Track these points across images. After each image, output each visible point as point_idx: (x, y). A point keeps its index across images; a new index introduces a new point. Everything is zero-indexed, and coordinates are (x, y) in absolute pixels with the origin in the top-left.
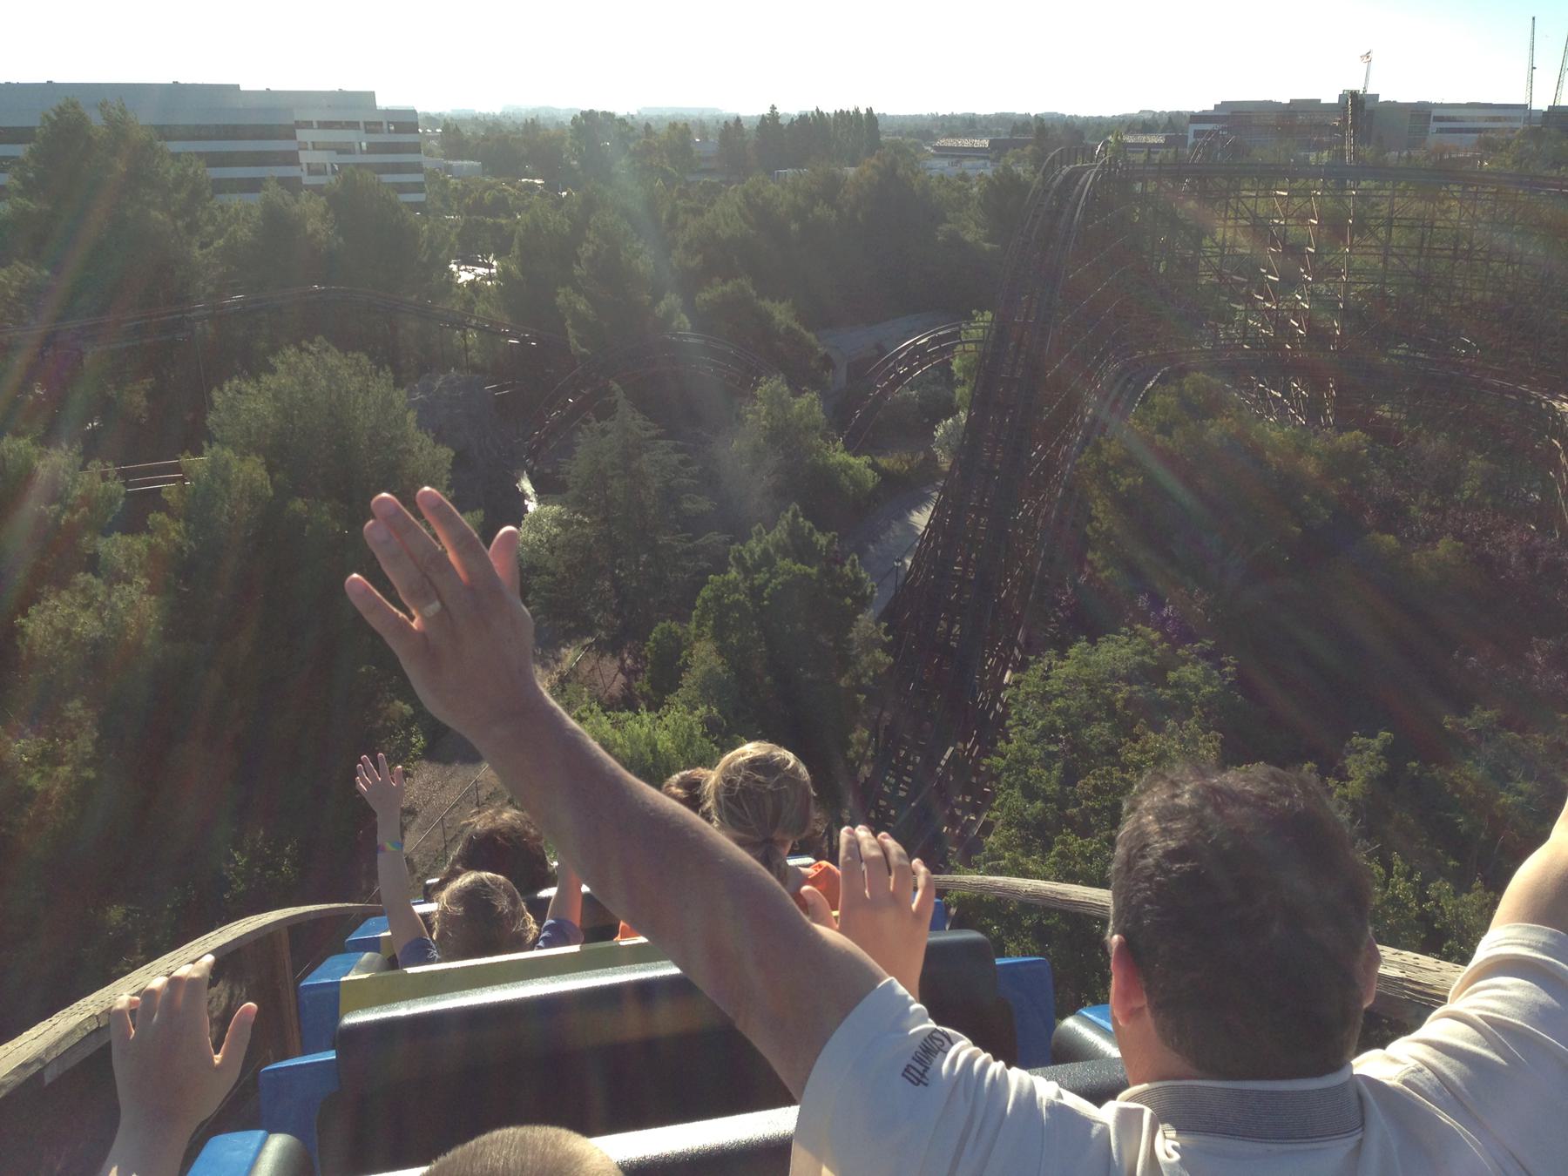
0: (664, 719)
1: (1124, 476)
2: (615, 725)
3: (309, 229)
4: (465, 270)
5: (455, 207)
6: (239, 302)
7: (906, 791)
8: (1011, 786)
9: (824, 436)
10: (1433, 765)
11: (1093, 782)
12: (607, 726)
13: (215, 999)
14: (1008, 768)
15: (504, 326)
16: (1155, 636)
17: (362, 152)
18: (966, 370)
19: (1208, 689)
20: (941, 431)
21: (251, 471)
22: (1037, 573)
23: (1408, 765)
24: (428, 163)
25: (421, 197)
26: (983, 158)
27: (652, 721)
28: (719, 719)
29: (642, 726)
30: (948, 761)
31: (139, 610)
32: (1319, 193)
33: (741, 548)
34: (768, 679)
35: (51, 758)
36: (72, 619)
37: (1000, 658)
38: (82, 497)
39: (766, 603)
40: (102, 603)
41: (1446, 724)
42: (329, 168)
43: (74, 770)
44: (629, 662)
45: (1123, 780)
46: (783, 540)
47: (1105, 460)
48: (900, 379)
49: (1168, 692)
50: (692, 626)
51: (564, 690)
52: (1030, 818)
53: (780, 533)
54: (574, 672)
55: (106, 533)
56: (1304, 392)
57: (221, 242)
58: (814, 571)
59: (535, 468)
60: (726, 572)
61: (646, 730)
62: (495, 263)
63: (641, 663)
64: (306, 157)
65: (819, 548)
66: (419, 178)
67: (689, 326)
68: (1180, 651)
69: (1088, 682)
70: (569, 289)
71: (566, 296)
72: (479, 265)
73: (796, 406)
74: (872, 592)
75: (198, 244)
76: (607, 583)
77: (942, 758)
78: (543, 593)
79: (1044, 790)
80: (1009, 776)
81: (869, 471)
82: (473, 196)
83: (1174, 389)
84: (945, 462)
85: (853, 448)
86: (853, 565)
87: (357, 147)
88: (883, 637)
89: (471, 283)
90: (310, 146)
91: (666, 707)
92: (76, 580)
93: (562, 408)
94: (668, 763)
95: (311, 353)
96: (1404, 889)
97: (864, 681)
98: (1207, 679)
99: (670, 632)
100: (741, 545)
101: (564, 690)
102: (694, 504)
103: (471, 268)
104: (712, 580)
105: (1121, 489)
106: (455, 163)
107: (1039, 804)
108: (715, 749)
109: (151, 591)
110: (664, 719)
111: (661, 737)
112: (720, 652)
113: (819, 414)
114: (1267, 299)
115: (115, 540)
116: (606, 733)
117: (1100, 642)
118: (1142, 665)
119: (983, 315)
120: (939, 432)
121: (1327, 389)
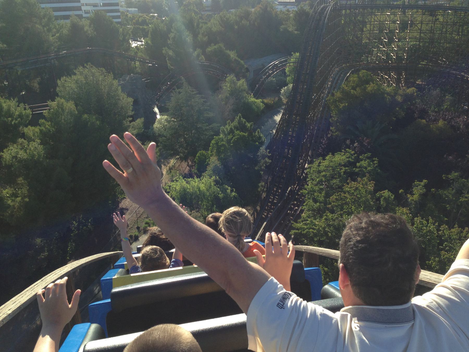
0: (202, 180)
1: (342, 103)
3: (85, 29)
4: (134, 43)
5: (130, 23)
6: (65, 53)
8: (309, 199)
9: (247, 93)
10: (439, 190)
11: (335, 197)
12: (185, 183)
14: (308, 193)
15: (147, 60)
16: (353, 152)
17: (101, 6)
20: (283, 91)
24: (121, 9)
25: (119, 20)
26: (293, 5)
27: (198, 181)
29: (195, 183)
30: (289, 191)
31: (38, 150)
32: (400, 13)
33: (224, 128)
34: (233, 168)
35: (15, 195)
36: (17, 153)
38: (19, 115)
39: (232, 144)
40: (27, 148)
41: (443, 177)
42: (91, 11)
44: (190, 163)
45: (344, 196)
48: (270, 75)
49: (357, 169)
50: (209, 152)
51: (171, 172)
52: (315, 208)
53: (236, 123)
54: (174, 166)
55: (26, 126)
58: (246, 134)
59: (159, 105)
60: (219, 135)
62: (143, 40)
64: (83, 8)
65: (248, 127)
66: (119, 14)
67: (204, 59)
68: (360, 157)
69: (332, 167)
70: (166, 48)
74: (264, 141)
75: (51, 35)
76: (182, 139)
78: (163, 143)
79: (319, 200)
80: (308, 196)
81: (261, 104)
84: (285, 100)
85: (256, 96)
86: (258, 132)
87: (99, 5)
89: (136, 47)
90: (85, 5)
94: (204, 194)
95: (87, 68)
97: (263, 167)
98: (369, 165)
99: (203, 154)
101: (171, 172)
103: (136, 42)
105: (341, 107)
106: (130, 9)
107: (318, 204)
108: (218, 189)
109: (41, 144)
110: (202, 180)
113: (245, 86)
114: (384, 47)
115: (29, 128)
116: (184, 185)
118: (349, 161)
119: (295, 54)
120: (282, 91)
121: (402, 75)
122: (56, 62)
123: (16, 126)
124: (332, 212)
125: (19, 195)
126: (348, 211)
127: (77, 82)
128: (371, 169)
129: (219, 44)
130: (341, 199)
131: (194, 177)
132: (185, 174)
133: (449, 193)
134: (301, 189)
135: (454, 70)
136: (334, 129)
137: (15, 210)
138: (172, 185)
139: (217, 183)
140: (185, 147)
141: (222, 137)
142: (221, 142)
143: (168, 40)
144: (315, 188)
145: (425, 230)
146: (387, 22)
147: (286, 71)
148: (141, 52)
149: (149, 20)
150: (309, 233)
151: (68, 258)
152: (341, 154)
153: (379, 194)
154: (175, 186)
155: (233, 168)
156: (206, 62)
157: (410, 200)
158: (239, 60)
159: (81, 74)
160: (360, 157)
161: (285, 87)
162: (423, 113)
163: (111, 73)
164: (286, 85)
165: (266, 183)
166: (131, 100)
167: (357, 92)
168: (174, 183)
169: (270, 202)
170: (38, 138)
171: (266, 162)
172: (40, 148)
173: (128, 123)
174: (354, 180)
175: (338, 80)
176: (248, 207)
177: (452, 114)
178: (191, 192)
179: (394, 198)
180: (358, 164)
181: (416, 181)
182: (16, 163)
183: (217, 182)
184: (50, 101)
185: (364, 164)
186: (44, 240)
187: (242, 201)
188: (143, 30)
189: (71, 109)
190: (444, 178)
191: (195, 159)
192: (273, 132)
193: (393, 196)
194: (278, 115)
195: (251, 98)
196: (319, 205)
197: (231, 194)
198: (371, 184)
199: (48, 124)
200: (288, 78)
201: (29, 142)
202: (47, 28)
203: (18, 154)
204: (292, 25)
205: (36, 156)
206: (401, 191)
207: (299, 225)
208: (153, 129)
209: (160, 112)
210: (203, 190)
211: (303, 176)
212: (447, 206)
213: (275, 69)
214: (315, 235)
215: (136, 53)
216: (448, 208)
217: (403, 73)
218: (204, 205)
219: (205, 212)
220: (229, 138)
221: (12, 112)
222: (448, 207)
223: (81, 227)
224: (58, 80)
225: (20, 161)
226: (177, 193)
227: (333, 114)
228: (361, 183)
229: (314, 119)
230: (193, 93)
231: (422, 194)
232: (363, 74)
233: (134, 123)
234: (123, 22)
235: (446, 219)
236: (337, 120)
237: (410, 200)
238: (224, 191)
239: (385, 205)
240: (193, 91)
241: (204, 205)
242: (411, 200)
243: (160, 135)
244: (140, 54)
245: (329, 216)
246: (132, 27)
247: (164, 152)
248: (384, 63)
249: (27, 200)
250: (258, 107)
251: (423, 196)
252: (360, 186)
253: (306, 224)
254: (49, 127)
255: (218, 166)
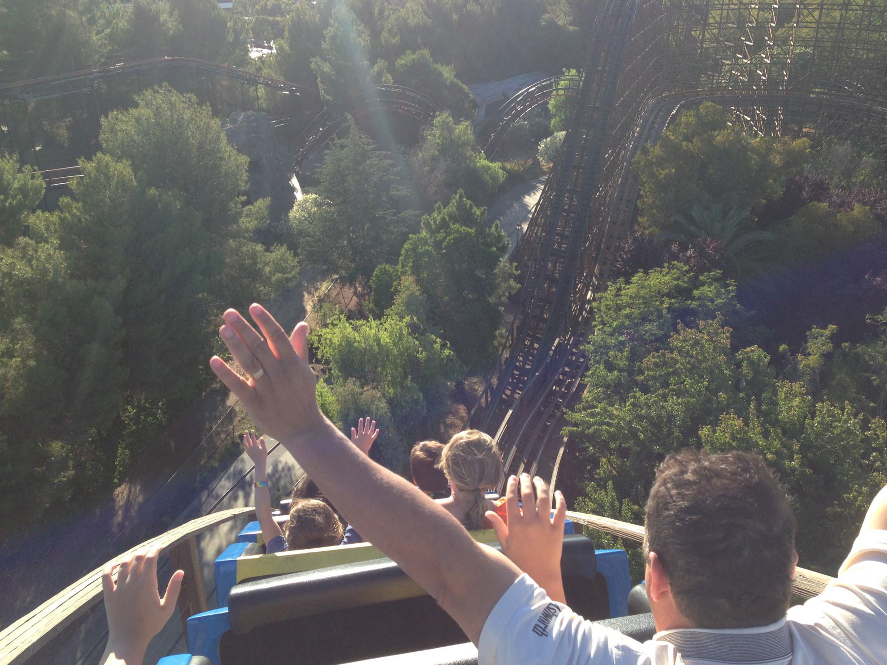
0: (384, 324)
2: (355, 329)
3: (162, 19)
4: (257, 51)
6: (121, 68)
7: (530, 365)
8: (598, 362)
10: (858, 345)
12: (350, 329)
13: (120, 495)
14: (596, 351)
18: (556, 106)
19: (720, 301)
21: (122, 169)
22: (606, 231)
23: (842, 345)
27: (377, 326)
28: (418, 324)
29: (371, 328)
30: (556, 347)
31: (54, 260)
33: (428, 217)
34: (446, 298)
36: (12, 266)
37: (585, 285)
39: (444, 251)
40: (32, 256)
41: (867, 319)
43: (22, 361)
44: (359, 289)
45: (672, 358)
46: (454, 212)
47: (650, 159)
49: (694, 303)
50: (399, 267)
51: (321, 307)
52: (610, 382)
53: (452, 208)
54: (327, 296)
56: (764, 117)
57: (109, 30)
58: (473, 231)
59: (300, 172)
61: (373, 331)
62: (274, 46)
63: (366, 290)
68: (701, 278)
69: (643, 298)
70: (318, 58)
71: (316, 63)
72: (264, 47)
73: (457, 131)
74: (508, 244)
75: (95, 32)
76: (345, 242)
77: (553, 345)
78: (307, 248)
80: (595, 356)
81: (501, 171)
82: (261, 4)
83: (692, 113)
84: (546, 165)
85: (491, 157)
86: (497, 227)
88: (515, 272)
89: (260, 58)
91: (385, 317)
92: (19, 242)
93: (316, 135)
94: (387, 351)
95: (160, 94)
96: (853, 424)
97: (503, 299)
98: (718, 294)
99: (385, 271)
100: (428, 215)
101: (321, 307)
102: (397, 191)
103: (260, 49)
104: (411, 238)
105: (661, 177)
107: (616, 373)
108: (416, 342)
109: (60, 247)
110: (384, 324)
111: (383, 336)
112: (418, 282)
113: (470, 136)
114: (745, 57)
115: (38, 215)
116: (349, 334)
117: (651, 272)
118: (677, 286)
119: (569, 71)
120: (541, 147)
121: (777, 115)
122: (104, 86)
123: (14, 212)
124: (645, 390)
125: (16, 354)
126: (679, 388)
127: (138, 120)
128: (722, 303)
129: (422, 51)
130: (665, 364)
131: (368, 317)
132: (350, 311)
133: (878, 352)
134: (581, 343)
135: (880, 104)
136: (646, 221)
137: (7, 385)
138: (325, 334)
139: (414, 329)
140: (350, 256)
141: (425, 236)
142: (422, 246)
143: (322, 42)
144: (609, 341)
145: (839, 429)
146: (753, 6)
147: (550, 106)
148: (270, 66)
149: (287, 5)
150: (599, 434)
151: (116, 480)
152: (661, 272)
153: (741, 354)
154: (329, 336)
155: (446, 298)
156: (396, 88)
157: (801, 366)
158: (460, 83)
159: (148, 105)
160: (701, 278)
161: (546, 139)
162: (820, 190)
163: (208, 104)
164: (548, 133)
165: (511, 332)
166: (244, 159)
167: (694, 146)
168: (328, 330)
169: (517, 368)
170: (56, 236)
171: (510, 288)
172: (59, 255)
173: (239, 206)
174: (688, 325)
175: (653, 123)
176: (473, 378)
177: (876, 193)
178: (363, 348)
179: (770, 363)
180: (696, 293)
181: (814, 328)
182: (11, 288)
183: (413, 328)
184: (83, 158)
185: (709, 293)
186: (67, 444)
187: (464, 367)
188: (275, 24)
189: (125, 176)
190: (868, 321)
191: (371, 281)
192: (522, 228)
193: (769, 357)
194: (532, 194)
195: (480, 159)
196: (617, 376)
197: (441, 352)
198: (724, 333)
199: (76, 208)
200: (553, 121)
201: (38, 242)
202: (89, 16)
203: (14, 270)
204: (565, 13)
205: (50, 272)
206: (782, 348)
207: (578, 416)
208: (289, 220)
209: (302, 186)
210: (387, 344)
211: (583, 317)
212: (874, 378)
213: (529, 101)
214: (613, 437)
215: (259, 69)
216: (875, 383)
217: (780, 110)
218: (387, 374)
219: (389, 389)
220: (438, 239)
221: (6, 183)
222: (874, 380)
223: (142, 417)
224: (103, 116)
225: (20, 283)
226: (334, 349)
227: (644, 191)
228: (705, 331)
229: (605, 202)
230: (370, 147)
231: (825, 353)
232: (708, 109)
233: (251, 207)
234: (236, 8)
235: (872, 404)
236: (653, 202)
237: (801, 366)
238: (428, 346)
239: (751, 375)
240: (368, 144)
241: (387, 374)
242: (805, 366)
243: (300, 233)
244: (265, 71)
245: (639, 398)
246: (253, 19)
247: (310, 267)
248: (744, 89)
249: (32, 363)
250: (494, 179)
251: (827, 357)
252: (703, 337)
253: (593, 415)
254: (78, 214)
255: (416, 296)
